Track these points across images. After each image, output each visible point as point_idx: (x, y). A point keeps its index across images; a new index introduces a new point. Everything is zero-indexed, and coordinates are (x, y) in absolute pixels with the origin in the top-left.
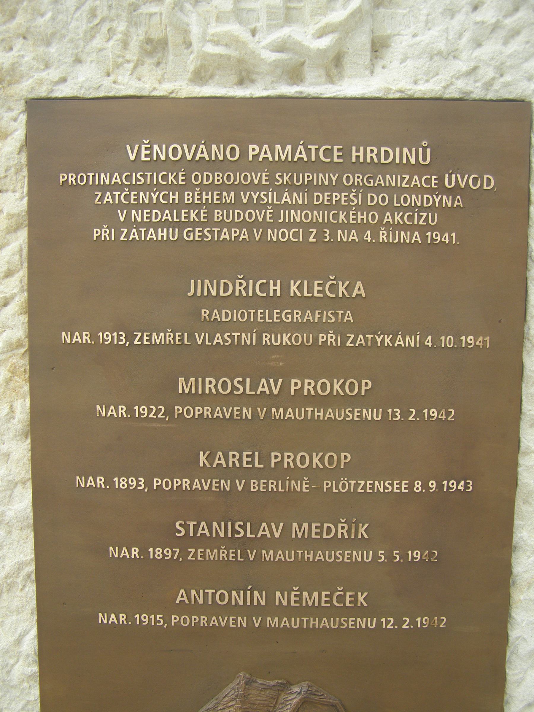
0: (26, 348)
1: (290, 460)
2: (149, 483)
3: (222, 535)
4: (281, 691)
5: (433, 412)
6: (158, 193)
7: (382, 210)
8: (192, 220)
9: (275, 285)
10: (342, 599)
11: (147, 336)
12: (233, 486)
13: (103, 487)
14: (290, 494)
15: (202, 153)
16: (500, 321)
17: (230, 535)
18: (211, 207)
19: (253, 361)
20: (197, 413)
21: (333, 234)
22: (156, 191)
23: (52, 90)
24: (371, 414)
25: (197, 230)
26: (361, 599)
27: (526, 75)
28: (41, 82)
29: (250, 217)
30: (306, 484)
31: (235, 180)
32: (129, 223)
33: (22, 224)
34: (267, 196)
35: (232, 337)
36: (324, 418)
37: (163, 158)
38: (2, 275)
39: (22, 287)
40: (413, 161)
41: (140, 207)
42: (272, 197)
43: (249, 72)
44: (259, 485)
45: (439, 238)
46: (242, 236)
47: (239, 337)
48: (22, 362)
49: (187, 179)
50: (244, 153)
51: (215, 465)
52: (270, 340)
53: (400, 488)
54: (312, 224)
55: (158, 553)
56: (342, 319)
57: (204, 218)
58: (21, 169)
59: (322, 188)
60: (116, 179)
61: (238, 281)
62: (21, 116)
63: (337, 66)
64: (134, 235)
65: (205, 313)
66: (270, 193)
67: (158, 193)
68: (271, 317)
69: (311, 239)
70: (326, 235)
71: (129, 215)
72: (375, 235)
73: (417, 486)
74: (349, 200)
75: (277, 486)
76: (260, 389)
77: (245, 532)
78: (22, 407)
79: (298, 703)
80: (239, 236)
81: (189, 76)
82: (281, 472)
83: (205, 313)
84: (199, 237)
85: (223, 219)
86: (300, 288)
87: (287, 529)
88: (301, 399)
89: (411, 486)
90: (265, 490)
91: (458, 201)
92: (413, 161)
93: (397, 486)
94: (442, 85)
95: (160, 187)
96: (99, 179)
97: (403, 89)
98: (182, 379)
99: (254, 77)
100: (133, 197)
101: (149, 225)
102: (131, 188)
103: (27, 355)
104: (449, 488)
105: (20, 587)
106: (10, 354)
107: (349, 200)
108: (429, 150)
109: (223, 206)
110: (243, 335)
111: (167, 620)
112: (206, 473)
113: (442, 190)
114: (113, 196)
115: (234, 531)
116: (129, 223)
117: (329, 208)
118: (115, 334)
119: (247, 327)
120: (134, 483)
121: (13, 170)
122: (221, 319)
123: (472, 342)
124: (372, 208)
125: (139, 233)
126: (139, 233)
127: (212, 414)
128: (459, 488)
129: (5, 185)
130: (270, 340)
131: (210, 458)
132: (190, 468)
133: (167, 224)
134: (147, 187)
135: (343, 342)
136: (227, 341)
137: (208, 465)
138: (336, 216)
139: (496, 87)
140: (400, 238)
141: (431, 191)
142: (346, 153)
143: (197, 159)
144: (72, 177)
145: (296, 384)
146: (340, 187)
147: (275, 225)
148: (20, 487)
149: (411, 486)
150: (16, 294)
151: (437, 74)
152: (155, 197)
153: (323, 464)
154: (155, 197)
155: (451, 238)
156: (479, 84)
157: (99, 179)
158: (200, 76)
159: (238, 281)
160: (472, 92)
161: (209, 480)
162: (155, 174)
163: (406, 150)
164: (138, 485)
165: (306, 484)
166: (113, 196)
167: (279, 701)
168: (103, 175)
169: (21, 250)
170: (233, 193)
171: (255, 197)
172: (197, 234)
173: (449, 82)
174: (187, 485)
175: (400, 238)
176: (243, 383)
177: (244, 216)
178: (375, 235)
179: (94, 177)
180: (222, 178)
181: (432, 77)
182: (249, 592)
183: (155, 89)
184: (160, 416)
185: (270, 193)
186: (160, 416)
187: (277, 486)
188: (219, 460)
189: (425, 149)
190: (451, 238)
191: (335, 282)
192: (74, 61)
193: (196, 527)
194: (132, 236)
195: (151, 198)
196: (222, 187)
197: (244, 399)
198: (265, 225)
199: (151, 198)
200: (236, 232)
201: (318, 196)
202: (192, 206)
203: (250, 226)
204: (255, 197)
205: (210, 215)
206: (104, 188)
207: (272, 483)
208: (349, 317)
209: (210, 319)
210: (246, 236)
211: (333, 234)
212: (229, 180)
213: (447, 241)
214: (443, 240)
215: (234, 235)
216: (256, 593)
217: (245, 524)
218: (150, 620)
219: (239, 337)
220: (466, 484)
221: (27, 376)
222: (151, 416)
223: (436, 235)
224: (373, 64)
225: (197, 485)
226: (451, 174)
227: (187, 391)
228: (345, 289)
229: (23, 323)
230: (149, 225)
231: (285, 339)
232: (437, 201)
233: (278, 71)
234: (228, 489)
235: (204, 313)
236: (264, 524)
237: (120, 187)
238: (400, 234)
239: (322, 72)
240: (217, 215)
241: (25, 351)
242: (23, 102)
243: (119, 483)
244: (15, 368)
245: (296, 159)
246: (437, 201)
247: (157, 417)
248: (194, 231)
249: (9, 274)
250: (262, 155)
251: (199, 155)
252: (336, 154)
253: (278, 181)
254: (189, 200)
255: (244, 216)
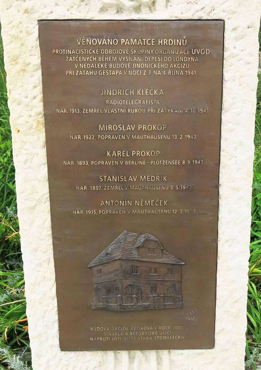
0: (43, 115)
1: (96, 111)
2: (89, 163)
3: (116, 181)
4: (138, 236)
5: (189, 136)
6: (89, 57)
7: (169, 63)
8: (101, 67)
9: (132, 91)
10: (158, 203)
11: (87, 110)
12: (119, 163)
13: (80, 139)
14: (139, 165)
15: (104, 42)
16: (212, 103)
17: (118, 181)
18: (108, 62)
19: (126, 118)
20: (106, 137)
21: (152, 72)
22: (88, 57)
23: (48, 17)
24: (167, 137)
25: (104, 71)
26: (165, 203)
27: (222, 10)
28: (43, 13)
29: (122, 66)
30: (145, 162)
31: (117, 52)
32: (79, 69)
33: (39, 68)
34: (128, 58)
35: (117, 110)
36: (150, 139)
37: (90, 44)
38: (32, 88)
39: (40, 92)
40: (180, 44)
41: (83, 62)
42: (130, 59)
43: (121, 8)
44: (128, 163)
45: (190, 73)
46: (120, 73)
47: (120, 110)
48: (42, 120)
49: (99, 51)
50: (120, 42)
51: (113, 156)
52: (131, 111)
53: (177, 163)
54: (144, 69)
55: (93, 188)
56: (156, 103)
57: (106, 67)
58: (37, 47)
59: (148, 55)
60: (73, 52)
61: (119, 90)
62: (36, 26)
63: (153, 5)
64: (81, 73)
65: (107, 101)
66: (129, 57)
67: (89, 57)
68: (131, 103)
69: (144, 74)
70: (78, 111)
71: (79, 66)
72: (167, 72)
73: (183, 162)
74: (157, 59)
75: (134, 163)
76: (128, 129)
77: (124, 179)
78: (42, 136)
79: (144, 240)
80: (119, 73)
81: (99, 10)
82: (136, 158)
83: (107, 101)
84: (104, 74)
85: (113, 67)
86: (141, 92)
87: (138, 178)
88: (142, 132)
89: (181, 162)
90: (125, 156)
91: (197, 59)
92: (180, 44)
93: (176, 162)
94: (191, 14)
95: (89, 55)
96: (67, 52)
97: (177, 16)
98: (100, 126)
99: (123, 10)
100: (80, 59)
101: (86, 69)
102: (79, 55)
103: (44, 117)
104: (195, 163)
105: (44, 202)
106: (37, 117)
107: (157, 59)
108: (186, 40)
109: (113, 62)
110: (121, 109)
111: (97, 212)
112: (109, 159)
113: (191, 55)
114: (73, 59)
115: (120, 179)
116: (79, 69)
117: (151, 62)
118: (76, 110)
119: (122, 107)
120: (84, 163)
121: (34, 48)
122: (113, 104)
123: (202, 111)
124: (165, 62)
125: (83, 72)
126: (83, 72)
127: (111, 138)
128: (199, 163)
129: (31, 53)
130: (131, 111)
131: (111, 153)
132: (103, 156)
133: (93, 69)
134: (86, 55)
135: (156, 111)
136: (116, 112)
137: (110, 156)
138: (153, 66)
139: (211, 14)
140: (176, 73)
141: (188, 56)
142: (156, 42)
143: (103, 44)
144: (57, 51)
145: (140, 127)
146: (154, 55)
147: (131, 69)
148: (42, 165)
149: (181, 162)
150: (38, 95)
151: (190, 10)
152: (88, 59)
153: (150, 155)
154: (88, 59)
155: (194, 73)
156: (205, 14)
157: (67, 52)
158: (103, 10)
159: (119, 90)
160: (202, 17)
161: (111, 161)
162: (88, 50)
163: (178, 40)
164: (86, 164)
165: (145, 162)
166: (73, 59)
167: (138, 240)
168: (68, 50)
169: (39, 78)
170: (116, 58)
171: (124, 59)
172: (104, 73)
173: (194, 13)
174: (103, 163)
175: (176, 73)
176: (122, 127)
177: (120, 66)
178: (167, 72)
179: (65, 51)
180: (112, 52)
181: (188, 11)
182: (126, 201)
183: (86, 16)
184: (93, 139)
185: (129, 57)
186: (93, 139)
187: (134, 163)
188: (114, 153)
189: (184, 40)
190: (194, 73)
191: (153, 90)
192: (55, 5)
193: (107, 178)
194: (80, 73)
195: (86, 59)
196: (112, 55)
197: (122, 133)
198: (128, 69)
199: (86, 59)
200: (117, 72)
201: (146, 58)
202: (102, 62)
203: (123, 70)
204: (124, 59)
205: (108, 66)
206: (69, 55)
207: (133, 162)
208: (158, 102)
209: (109, 103)
210: (121, 73)
211: (152, 72)
212: (114, 52)
213: (193, 74)
214: (191, 74)
215: (117, 73)
216: (128, 201)
217: (124, 177)
218: (91, 212)
219: (120, 110)
220: (201, 162)
221: (44, 125)
222: (90, 139)
223: (189, 72)
224: (167, 4)
225: (106, 163)
226: (194, 49)
227: (102, 130)
228: (157, 92)
229: (41, 106)
230: (86, 69)
231: (136, 110)
232: (189, 59)
233: (131, 9)
234: (117, 164)
235: (107, 102)
236: (130, 177)
237: (75, 55)
238: (176, 72)
239: (148, 9)
240: (111, 66)
241: (43, 116)
242: (37, 21)
243: (79, 163)
244: (39, 122)
245: (138, 44)
246: (189, 59)
247: (92, 139)
248: (102, 72)
249: (35, 87)
250: (126, 43)
251: (103, 43)
252: (152, 42)
253: (132, 53)
254: (100, 60)
255: (120, 66)
